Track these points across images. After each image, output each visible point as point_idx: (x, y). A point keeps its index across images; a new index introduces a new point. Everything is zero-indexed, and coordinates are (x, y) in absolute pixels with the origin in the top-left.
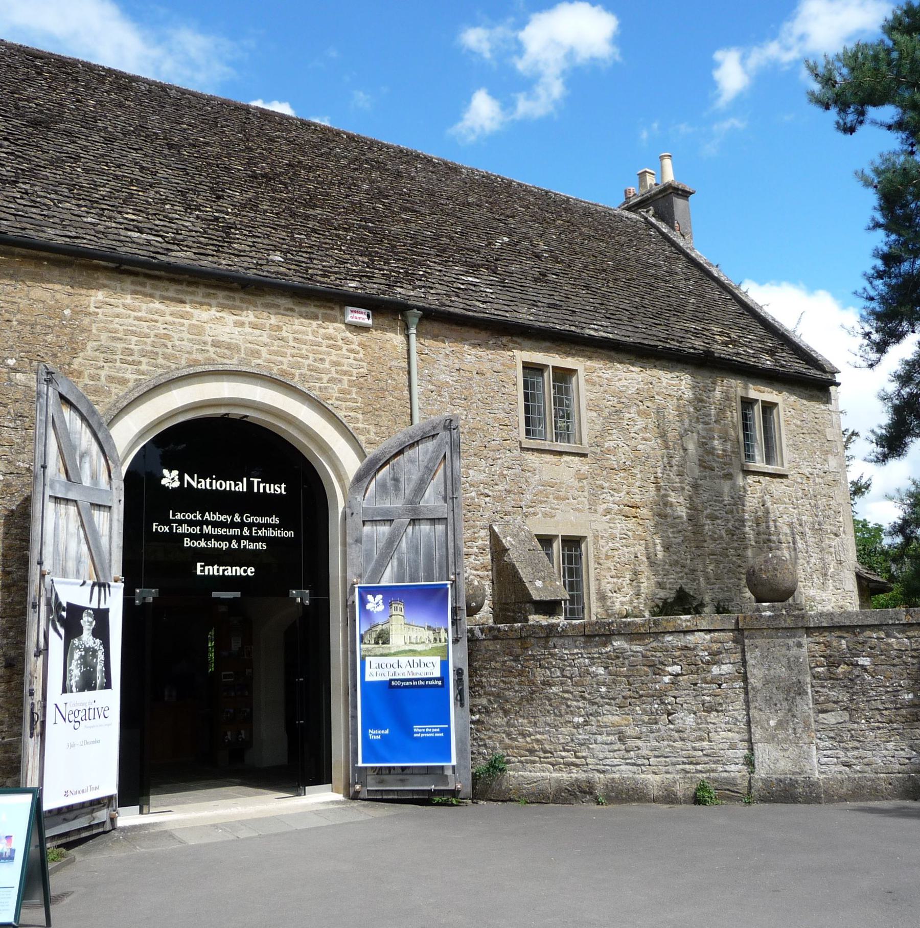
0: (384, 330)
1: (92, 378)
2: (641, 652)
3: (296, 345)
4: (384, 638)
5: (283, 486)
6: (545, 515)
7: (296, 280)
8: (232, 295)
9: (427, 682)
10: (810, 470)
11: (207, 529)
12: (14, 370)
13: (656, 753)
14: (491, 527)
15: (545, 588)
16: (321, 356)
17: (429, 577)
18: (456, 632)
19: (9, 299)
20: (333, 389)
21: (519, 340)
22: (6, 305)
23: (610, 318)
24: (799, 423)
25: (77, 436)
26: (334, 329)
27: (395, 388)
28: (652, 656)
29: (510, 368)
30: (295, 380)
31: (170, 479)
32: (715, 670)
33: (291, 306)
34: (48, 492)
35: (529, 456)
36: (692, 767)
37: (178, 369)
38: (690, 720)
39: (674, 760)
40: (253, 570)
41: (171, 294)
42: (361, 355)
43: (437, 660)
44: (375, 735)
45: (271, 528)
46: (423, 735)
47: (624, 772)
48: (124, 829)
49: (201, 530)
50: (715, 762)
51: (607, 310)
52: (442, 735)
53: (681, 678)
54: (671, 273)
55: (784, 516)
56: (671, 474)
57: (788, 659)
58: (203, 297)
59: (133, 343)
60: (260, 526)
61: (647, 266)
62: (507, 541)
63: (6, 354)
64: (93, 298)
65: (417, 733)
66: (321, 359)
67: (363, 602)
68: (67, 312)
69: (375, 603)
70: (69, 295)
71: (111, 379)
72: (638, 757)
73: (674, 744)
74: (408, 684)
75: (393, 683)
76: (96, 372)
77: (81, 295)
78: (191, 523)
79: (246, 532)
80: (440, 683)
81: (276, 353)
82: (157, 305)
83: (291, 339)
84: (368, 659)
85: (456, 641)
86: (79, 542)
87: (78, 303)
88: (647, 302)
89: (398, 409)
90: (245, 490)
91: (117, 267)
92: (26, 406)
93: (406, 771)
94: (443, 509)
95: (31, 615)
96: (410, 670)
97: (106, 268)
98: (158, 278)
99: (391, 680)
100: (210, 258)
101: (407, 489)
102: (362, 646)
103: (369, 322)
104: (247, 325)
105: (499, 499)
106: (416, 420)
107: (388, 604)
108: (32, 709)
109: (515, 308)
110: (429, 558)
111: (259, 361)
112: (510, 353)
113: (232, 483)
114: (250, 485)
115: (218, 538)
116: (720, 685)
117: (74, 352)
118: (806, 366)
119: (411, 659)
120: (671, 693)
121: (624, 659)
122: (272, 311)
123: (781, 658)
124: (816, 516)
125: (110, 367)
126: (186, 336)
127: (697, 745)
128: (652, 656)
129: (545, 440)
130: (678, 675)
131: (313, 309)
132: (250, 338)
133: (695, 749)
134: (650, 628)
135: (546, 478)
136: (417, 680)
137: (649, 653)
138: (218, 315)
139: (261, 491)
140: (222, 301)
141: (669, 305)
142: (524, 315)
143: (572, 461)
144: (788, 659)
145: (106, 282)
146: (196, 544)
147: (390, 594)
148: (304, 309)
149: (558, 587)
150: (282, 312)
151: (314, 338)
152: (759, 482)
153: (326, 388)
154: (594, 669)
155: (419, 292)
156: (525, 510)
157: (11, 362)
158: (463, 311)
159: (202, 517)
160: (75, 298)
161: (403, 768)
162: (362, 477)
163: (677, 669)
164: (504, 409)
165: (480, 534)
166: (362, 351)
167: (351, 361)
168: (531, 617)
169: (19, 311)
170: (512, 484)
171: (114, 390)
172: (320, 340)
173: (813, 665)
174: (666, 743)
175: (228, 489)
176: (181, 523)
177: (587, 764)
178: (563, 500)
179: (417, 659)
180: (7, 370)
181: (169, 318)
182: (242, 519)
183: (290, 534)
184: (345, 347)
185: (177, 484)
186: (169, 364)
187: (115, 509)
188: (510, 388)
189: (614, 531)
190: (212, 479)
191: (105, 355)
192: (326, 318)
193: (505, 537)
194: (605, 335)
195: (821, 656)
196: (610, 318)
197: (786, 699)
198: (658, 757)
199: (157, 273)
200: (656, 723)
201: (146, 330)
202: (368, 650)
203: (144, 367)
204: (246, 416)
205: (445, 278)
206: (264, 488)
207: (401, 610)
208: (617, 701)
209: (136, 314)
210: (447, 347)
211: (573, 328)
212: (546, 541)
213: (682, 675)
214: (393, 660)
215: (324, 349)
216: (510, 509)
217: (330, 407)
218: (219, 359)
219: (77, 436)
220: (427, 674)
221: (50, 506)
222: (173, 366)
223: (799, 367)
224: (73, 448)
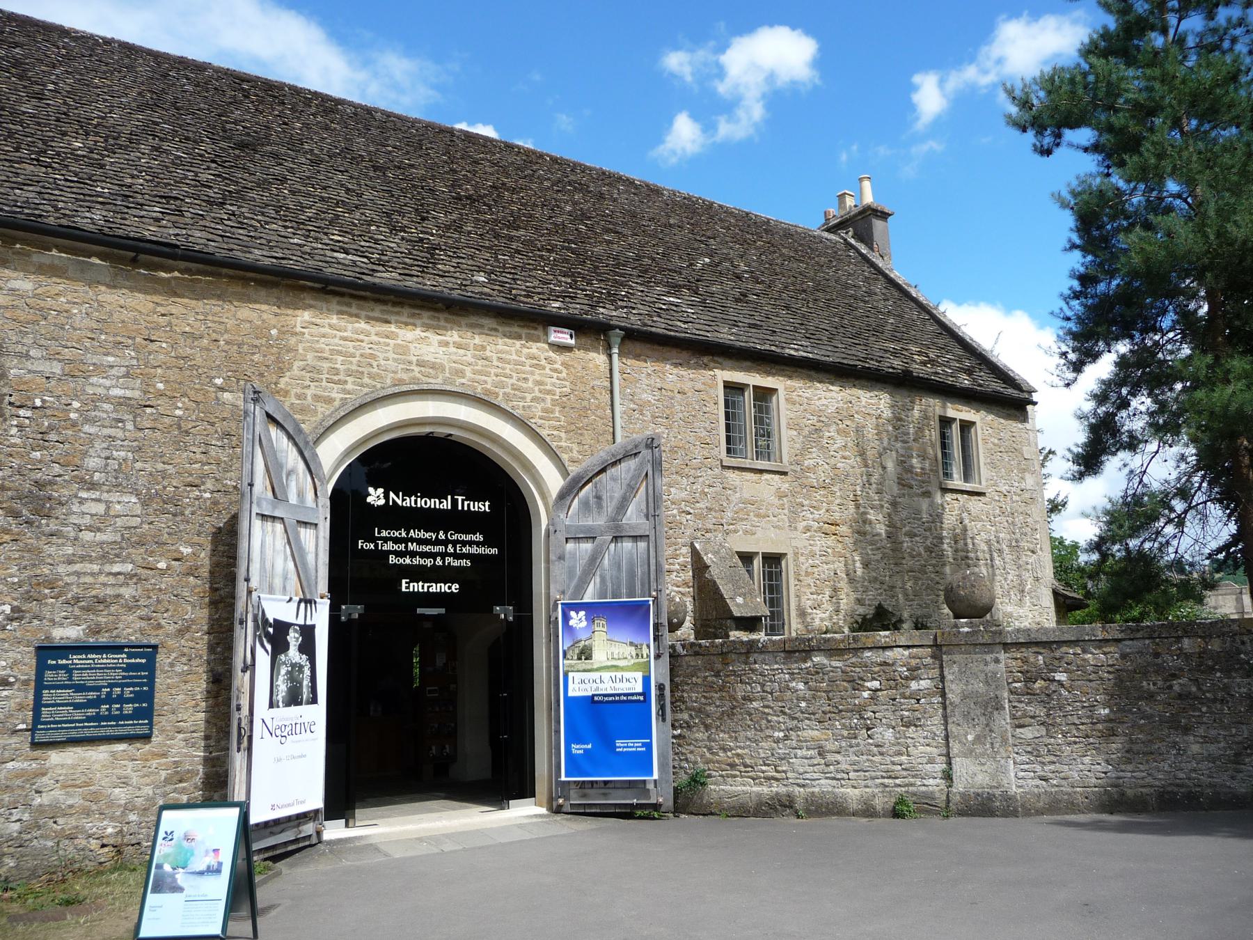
0: (587, 350)
1: (298, 397)
5: (487, 503)
6: (746, 532)
7: (500, 301)
11: (412, 547)
12: (222, 389)
15: (745, 604)
19: (216, 319)
26: (537, 349)
27: (598, 407)
31: (376, 497)
32: (914, 685)
34: (255, 510)
35: (730, 474)
36: (891, 781)
38: (889, 734)
39: (873, 774)
41: (376, 314)
42: (564, 375)
43: (639, 676)
44: (577, 749)
45: (475, 545)
47: (824, 786)
48: (330, 843)
49: (406, 547)
50: (913, 777)
53: (880, 693)
54: (870, 293)
60: (464, 543)
61: (846, 286)
62: (708, 558)
63: (214, 373)
67: (566, 618)
68: (274, 332)
71: (317, 398)
72: (837, 771)
78: (396, 541)
79: (450, 549)
80: (642, 698)
81: (480, 373)
82: (362, 325)
84: (571, 675)
85: (658, 657)
86: (286, 559)
89: (601, 428)
94: (644, 526)
97: (312, 289)
100: (415, 279)
101: (610, 507)
103: (573, 342)
105: (700, 517)
106: (619, 439)
107: (590, 620)
108: (239, 724)
111: (463, 381)
114: (455, 502)
115: (424, 555)
117: (281, 372)
119: (613, 674)
120: (870, 708)
126: (391, 355)
127: (896, 759)
131: (516, 329)
132: (454, 358)
133: (893, 763)
135: (746, 495)
136: (619, 695)
142: (725, 335)
145: (312, 302)
146: (401, 561)
147: (593, 610)
148: (507, 329)
153: (529, 407)
155: (622, 313)
157: (219, 381)
161: (606, 782)
162: (565, 495)
163: (876, 684)
166: (565, 371)
168: (731, 633)
171: (320, 409)
174: (865, 757)
176: (387, 541)
179: (619, 675)
181: (374, 338)
183: (494, 551)
184: (548, 366)
185: (382, 502)
187: (321, 526)
188: (710, 407)
199: (363, 293)
202: (571, 666)
203: (349, 387)
210: (649, 366)
211: (773, 348)
212: (746, 558)
213: (880, 690)
214: (595, 675)
215: (528, 368)
216: (711, 526)
221: (257, 523)
222: (379, 386)
223: (996, 386)
224: (280, 466)
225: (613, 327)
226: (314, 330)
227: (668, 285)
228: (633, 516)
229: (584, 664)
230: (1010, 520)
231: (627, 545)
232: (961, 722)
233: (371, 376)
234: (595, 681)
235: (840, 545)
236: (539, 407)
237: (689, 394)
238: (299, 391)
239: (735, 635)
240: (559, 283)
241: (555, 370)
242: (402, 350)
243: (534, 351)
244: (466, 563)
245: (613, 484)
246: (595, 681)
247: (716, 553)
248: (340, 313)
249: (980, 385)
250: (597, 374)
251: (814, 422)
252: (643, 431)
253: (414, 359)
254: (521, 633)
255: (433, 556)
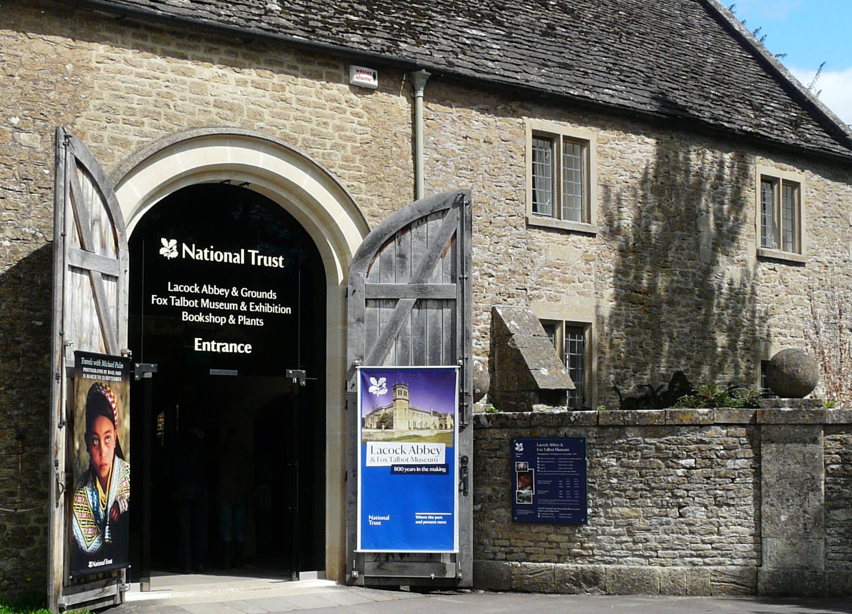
0: (390, 92)
1: (95, 139)
2: (654, 444)
3: (300, 107)
4: (387, 423)
5: (281, 259)
6: (550, 298)
7: (299, 36)
8: (234, 49)
9: (432, 469)
10: (829, 258)
11: (206, 303)
12: (18, 129)
13: (665, 545)
14: (494, 309)
15: (551, 376)
16: (325, 120)
17: (435, 360)
18: (462, 418)
19: (11, 52)
20: (336, 156)
21: (529, 106)
22: (9, 58)
23: (624, 81)
24: (821, 205)
25: (90, 203)
26: (338, 90)
27: (400, 156)
28: (666, 448)
29: (518, 137)
30: (298, 145)
31: (169, 249)
32: (730, 463)
33: (295, 64)
34: (68, 262)
35: (536, 234)
36: (700, 559)
37: (180, 131)
38: (700, 514)
39: (683, 552)
40: (250, 347)
41: (172, 48)
42: (365, 120)
43: (442, 447)
44: (375, 520)
45: (268, 304)
46: (425, 522)
47: (632, 564)
48: (131, 603)
49: (199, 304)
50: (722, 556)
51: (621, 71)
52: (445, 522)
53: (694, 471)
54: (687, 25)
55: (799, 308)
56: (682, 258)
57: (804, 455)
58: (205, 52)
59: (135, 102)
60: (257, 301)
61: (661, 16)
62: (511, 325)
63: (9, 112)
64: (94, 52)
65: (419, 520)
66: (324, 123)
67: (366, 385)
68: (69, 67)
69: (378, 387)
70: (71, 48)
71: (114, 140)
72: (646, 549)
73: (684, 537)
74: (412, 470)
75: (396, 469)
76: (100, 132)
77: (82, 48)
78: (190, 296)
79: (243, 307)
80: (444, 470)
81: (279, 116)
82: (158, 60)
83: (294, 100)
84: (369, 444)
85: (462, 428)
86: (91, 314)
87: (80, 59)
88: (662, 61)
89: (402, 179)
90: (243, 262)
91: (118, 18)
92: (31, 169)
93: (405, 559)
94: (451, 290)
95: (56, 386)
96: (414, 456)
97: (107, 19)
98: (160, 31)
99: (393, 466)
100: (208, 8)
101: (414, 265)
102: (363, 430)
103: (375, 83)
104: (250, 84)
105: (504, 280)
106: (422, 194)
107: (392, 387)
108: (57, 480)
109: (524, 67)
110: (435, 338)
111: (261, 124)
112: (520, 120)
113: (230, 254)
114: (248, 256)
115: (217, 313)
116: (733, 479)
118: (833, 141)
119: (415, 445)
120: (683, 486)
121: (637, 450)
122: (276, 68)
123: (797, 454)
124: (833, 309)
125: (113, 128)
126: (188, 95)
127: (707, 538)
128: (666, 448)
129: (553, 217)
130: (692, 468)
131: (317, 68)
132: (253, 99)
133: (703, 542)
134: (666, 420)
135: (552, 258)
136: (421, 466)
137: (663, 446)
138: (221, 72)
139: (259, 264)
140: (224, 57)
141: (686, 66)
142: (535, 78)
143: (580, 240)
144: (804, 455)
145: (107, 34)
146: (194, 318)
147: (394, 377)
148: (307, 67)
149: (564, 376)
150: (285, 69)
151: (317, 100)
152: (774, 269)
153: (329, 154)
154: (606, 460)
155: (424, 49)
156: (529, 292)
157: (15, 121)
158: (472, 72)
159: (200, 290)
160: (77, 52)
161: (402, 555)
162: (363, 254)
164: (511, 182)
165: (483, 317)
166: (366, 115)
167: (355, 126)
168: (534, 407)
169: (22, 65)
170: (517, 264)
171: (117, 153)
172: (324, 102)
173: (828, 462)
174: (675, 535)
175: (226, 261)
176: (180, 297)
177: (594, 555)
178: (569, 282)
179: (421, 445)
180: (11, 130)
181: (171, 76)
182: (239, 293)
183: (287, 310)
184: (349, 110)
185: (175, 254)
186: (171, 126)
187: (121, 280)
188: (518, 160)
189: (619, 318)
190: (210, 249)
191: (108, 114)
192: (332, 78)
193: (509, 321)
194: (621, 102)
195: (837, 453)
196: (624, 81)
197: (799, 495)
198: (667, 549)
199: (158, 25)
200: (666, 516)
201: (148, 88)
202: (369, 435)
203: (147, 129)
204: (247, 184)
205: (450, 31)
206: (262, 260)
207: (405, 394)
208: (628, 493)
209: (137, 70)
210: (454, 112)
211: (587, 93)
212: (550, 326)
213: (695, 468)
214: (396, 445)
215: (328, 112)
216: (514, 291)
217: (333, 176)
218: (221, 121)
219: (90, 203)
220: (432, 460)
221: (69, 273)
222: (176, 128)
223: (825, 141)
224: (86, 215)
225: (420, 68)
226: (111, 65)
227: (470, 14)
228: (439, 279)
229: (381, 434)
230: (829, 294)
231: (431, 312)
232: (775, 502)
233: (168, 118)
234: (395, 451)
235: (647, 317)
236: (339, 154)
237: (495, 144)
238: (96, 132)
239: (540, 408)
240: (355, 12)
241: (357, 115)
242: (199, 89)
243: (334, 92)
244: (258, 322)
245: (415, 244)
246: (395, 451)
247: (519, 320)
248: (136, 47)
249: (808, 141)
250: (400, 119)
251: (627, 178)
252: (453, 186)
253: (212, 99)
254: (314, 396)
255: (225, 313)
